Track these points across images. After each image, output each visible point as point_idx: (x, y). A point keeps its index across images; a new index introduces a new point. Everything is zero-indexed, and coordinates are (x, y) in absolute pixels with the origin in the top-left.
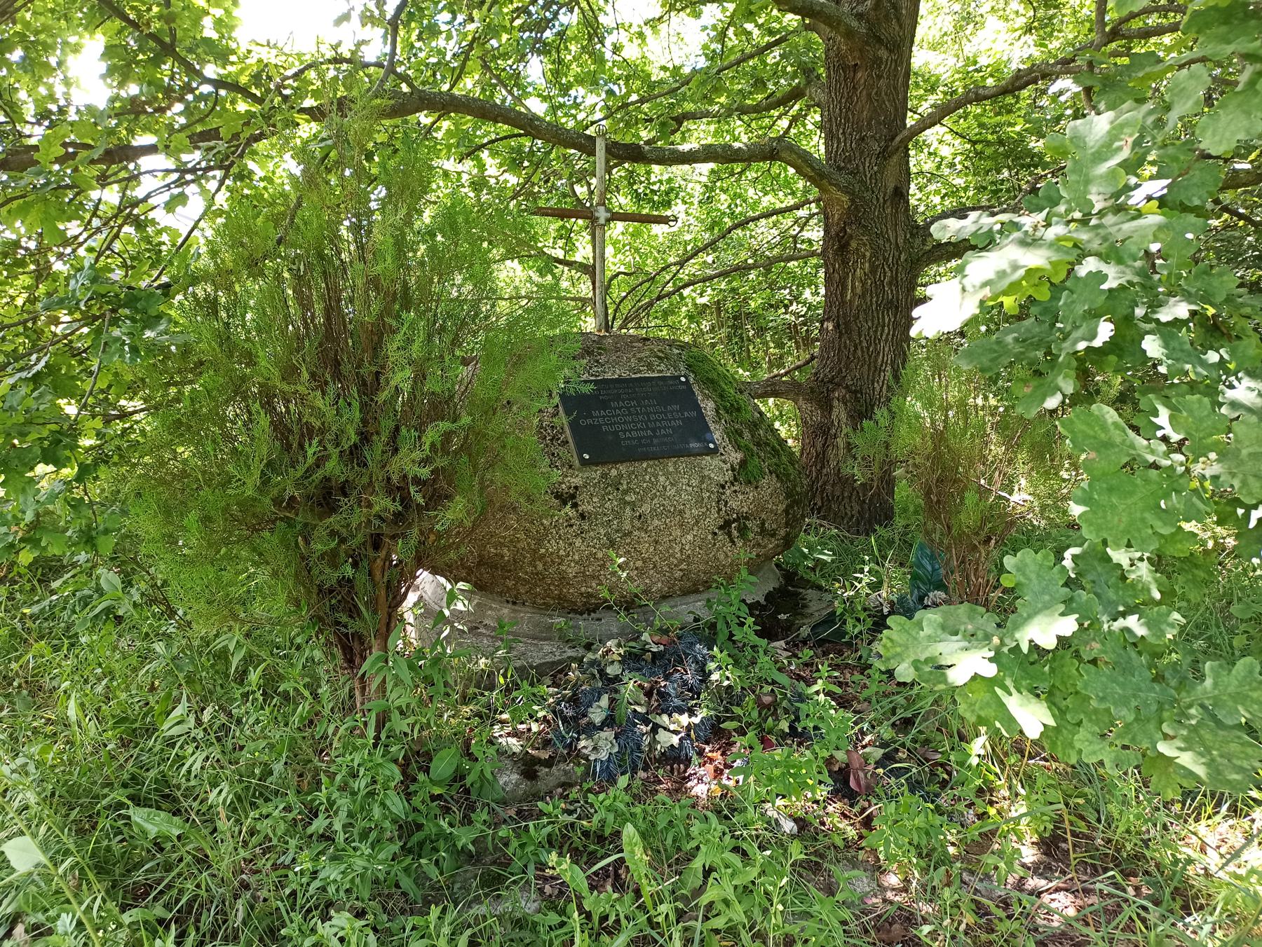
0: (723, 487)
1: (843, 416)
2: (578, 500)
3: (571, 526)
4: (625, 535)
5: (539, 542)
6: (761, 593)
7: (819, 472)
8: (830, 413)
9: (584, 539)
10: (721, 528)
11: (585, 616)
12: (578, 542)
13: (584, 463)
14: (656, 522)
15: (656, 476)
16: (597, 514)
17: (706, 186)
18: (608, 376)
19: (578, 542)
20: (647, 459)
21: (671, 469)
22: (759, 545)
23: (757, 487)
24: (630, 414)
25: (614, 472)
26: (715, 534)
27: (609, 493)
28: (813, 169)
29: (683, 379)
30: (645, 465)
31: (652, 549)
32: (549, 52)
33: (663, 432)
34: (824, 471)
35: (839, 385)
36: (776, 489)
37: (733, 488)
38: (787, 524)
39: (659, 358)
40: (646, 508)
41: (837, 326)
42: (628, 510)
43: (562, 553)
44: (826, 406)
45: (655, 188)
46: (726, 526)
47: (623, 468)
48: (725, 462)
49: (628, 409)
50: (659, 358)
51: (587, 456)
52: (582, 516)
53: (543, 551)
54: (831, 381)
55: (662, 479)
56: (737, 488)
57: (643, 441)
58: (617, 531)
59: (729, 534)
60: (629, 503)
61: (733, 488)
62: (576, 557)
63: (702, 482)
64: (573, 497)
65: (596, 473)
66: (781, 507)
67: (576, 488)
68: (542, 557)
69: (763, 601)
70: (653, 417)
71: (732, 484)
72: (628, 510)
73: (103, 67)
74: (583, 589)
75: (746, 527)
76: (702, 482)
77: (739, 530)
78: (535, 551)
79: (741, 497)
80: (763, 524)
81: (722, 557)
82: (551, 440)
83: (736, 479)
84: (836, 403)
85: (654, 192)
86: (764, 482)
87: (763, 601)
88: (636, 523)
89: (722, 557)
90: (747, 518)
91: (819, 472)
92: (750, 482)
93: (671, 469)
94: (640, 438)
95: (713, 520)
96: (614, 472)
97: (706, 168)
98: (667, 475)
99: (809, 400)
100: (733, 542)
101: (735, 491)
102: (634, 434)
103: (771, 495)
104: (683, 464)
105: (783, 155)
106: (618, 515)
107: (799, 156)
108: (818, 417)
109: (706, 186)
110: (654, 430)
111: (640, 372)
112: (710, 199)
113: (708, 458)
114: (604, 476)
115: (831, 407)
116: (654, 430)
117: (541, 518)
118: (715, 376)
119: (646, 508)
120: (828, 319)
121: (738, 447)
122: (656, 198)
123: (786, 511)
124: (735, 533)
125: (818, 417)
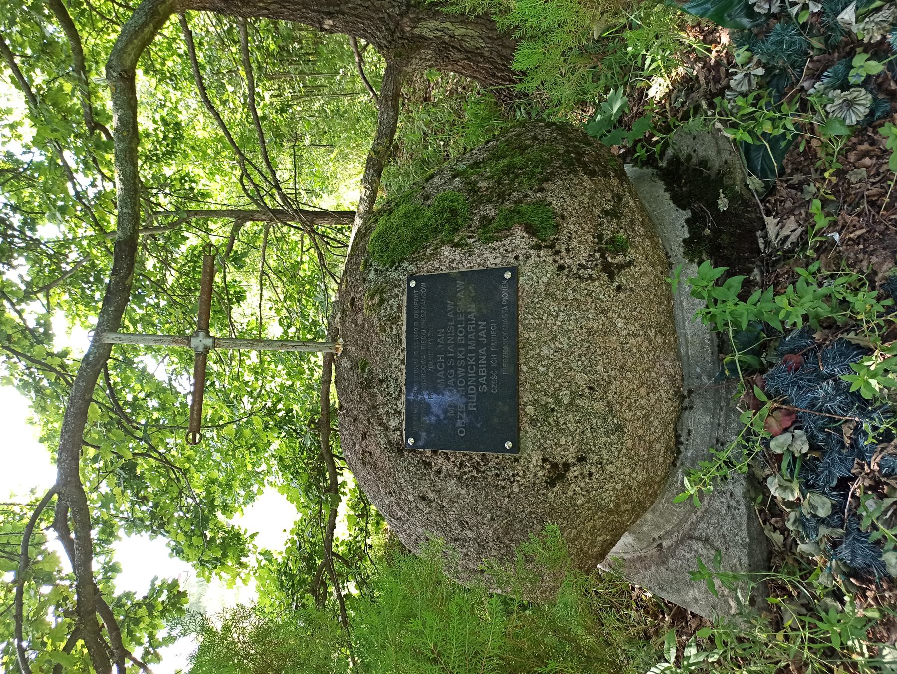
0: (561, 268)
1: (432, 24)
2: (560, 461)
3: (591, 474)
4: (611, 411)
5: (600, 508)
6: (674, 214)
7: (487, 60)
8: (426, 39)
9: (610, 462)
10: (611, 277)
11: (682, 448)
12: (611, 468)
13: (516, 448)
14: (599, 368)
15: (541, 358)
16: (580, 442)
17: (160, 80)
18: (402, 378)
19: (611, 468)
20: (517, 365)
21: (533, 335)
22: (632, 222)
23: (563, 217)
24: (455, 368)
25: (530, 410)
26: (619, 288)
27: (557, 422)
28: (145, 25)
29: (413, 284)
30: (524, 368)
31: (630, 376)
32: (33, 220)
33: (483, 333)
34: (487, 54)
35: (397, 24)
36: (564, 188)
37: (564, 253)
38: (606, 176)
39: (381, 302)
40: (581, 380)
41: (330, 15)
42: (579, 402)
43: (619, 486)
44: (419, 42)
45: (161, 135)
46: (610, 270)
47: (525, 397)
48: (528, 257)
49: (447, 368)
50: (381, 302)
51: (508, 445)
52: (581, 459)
53: (612, 506)
54: (392, 33)
55: (545, 351)
56: (563, 247)
57: (494, 365)
58: (605, 420)
59: (621, 267)
60: (572, 400)
61: (564, 253)
62: (628, 471)
63: (553, 296)
64: (555, 466)
65: (529, 433)
66: (588, 183)
67: (544, 460)
68: (618, 505)
69: (688, 214)
70: (461, 340)
71: (557, 253)
72: (579, 402)
73: (58, 555)
74: (661, 460)
75: (612, 241)
76: (553, 296)
77: (615, 253)
78: (610, 512)
79: (574, 243)
80: (606, 213)
81: (646, 280)
82: (478, 471)
83: (552, 246)
84: (417, 31)
85: (166, 137)
86: (555, 204)
87: (688, 214)
88: (598, 394)
89: (646, 280)
90: (600, 237)
91: (487, 60)
92: (556, 226)
93: (533, 335)
94: (489, 367)
95: (601, 288)
96: (530, 410)
97: (143, 81)
98: (541, 343)
99: (408, 59)
100: (630, 263)
101: (567, 250)
102: (483, 372)
103: (572, 196)
104: (526, 318)
105: (128, 63)
106: (586, 417)
107: (129, 42)
108: (428, 53)
109: (160, 80)
110: (480, 345)
111: (398, 335)
112: (173, 77)
113: (521, 280)
114: (533, 422)
115: (421, 37)
116: (480, 345)
117: (575, 505)
118: (405, 232)
119: (581, 380)
120: (321, 23)
121: (506, 230)
122: (171, 135)
123: (592, 174)
124: (619, 259)
125: (428, 53)
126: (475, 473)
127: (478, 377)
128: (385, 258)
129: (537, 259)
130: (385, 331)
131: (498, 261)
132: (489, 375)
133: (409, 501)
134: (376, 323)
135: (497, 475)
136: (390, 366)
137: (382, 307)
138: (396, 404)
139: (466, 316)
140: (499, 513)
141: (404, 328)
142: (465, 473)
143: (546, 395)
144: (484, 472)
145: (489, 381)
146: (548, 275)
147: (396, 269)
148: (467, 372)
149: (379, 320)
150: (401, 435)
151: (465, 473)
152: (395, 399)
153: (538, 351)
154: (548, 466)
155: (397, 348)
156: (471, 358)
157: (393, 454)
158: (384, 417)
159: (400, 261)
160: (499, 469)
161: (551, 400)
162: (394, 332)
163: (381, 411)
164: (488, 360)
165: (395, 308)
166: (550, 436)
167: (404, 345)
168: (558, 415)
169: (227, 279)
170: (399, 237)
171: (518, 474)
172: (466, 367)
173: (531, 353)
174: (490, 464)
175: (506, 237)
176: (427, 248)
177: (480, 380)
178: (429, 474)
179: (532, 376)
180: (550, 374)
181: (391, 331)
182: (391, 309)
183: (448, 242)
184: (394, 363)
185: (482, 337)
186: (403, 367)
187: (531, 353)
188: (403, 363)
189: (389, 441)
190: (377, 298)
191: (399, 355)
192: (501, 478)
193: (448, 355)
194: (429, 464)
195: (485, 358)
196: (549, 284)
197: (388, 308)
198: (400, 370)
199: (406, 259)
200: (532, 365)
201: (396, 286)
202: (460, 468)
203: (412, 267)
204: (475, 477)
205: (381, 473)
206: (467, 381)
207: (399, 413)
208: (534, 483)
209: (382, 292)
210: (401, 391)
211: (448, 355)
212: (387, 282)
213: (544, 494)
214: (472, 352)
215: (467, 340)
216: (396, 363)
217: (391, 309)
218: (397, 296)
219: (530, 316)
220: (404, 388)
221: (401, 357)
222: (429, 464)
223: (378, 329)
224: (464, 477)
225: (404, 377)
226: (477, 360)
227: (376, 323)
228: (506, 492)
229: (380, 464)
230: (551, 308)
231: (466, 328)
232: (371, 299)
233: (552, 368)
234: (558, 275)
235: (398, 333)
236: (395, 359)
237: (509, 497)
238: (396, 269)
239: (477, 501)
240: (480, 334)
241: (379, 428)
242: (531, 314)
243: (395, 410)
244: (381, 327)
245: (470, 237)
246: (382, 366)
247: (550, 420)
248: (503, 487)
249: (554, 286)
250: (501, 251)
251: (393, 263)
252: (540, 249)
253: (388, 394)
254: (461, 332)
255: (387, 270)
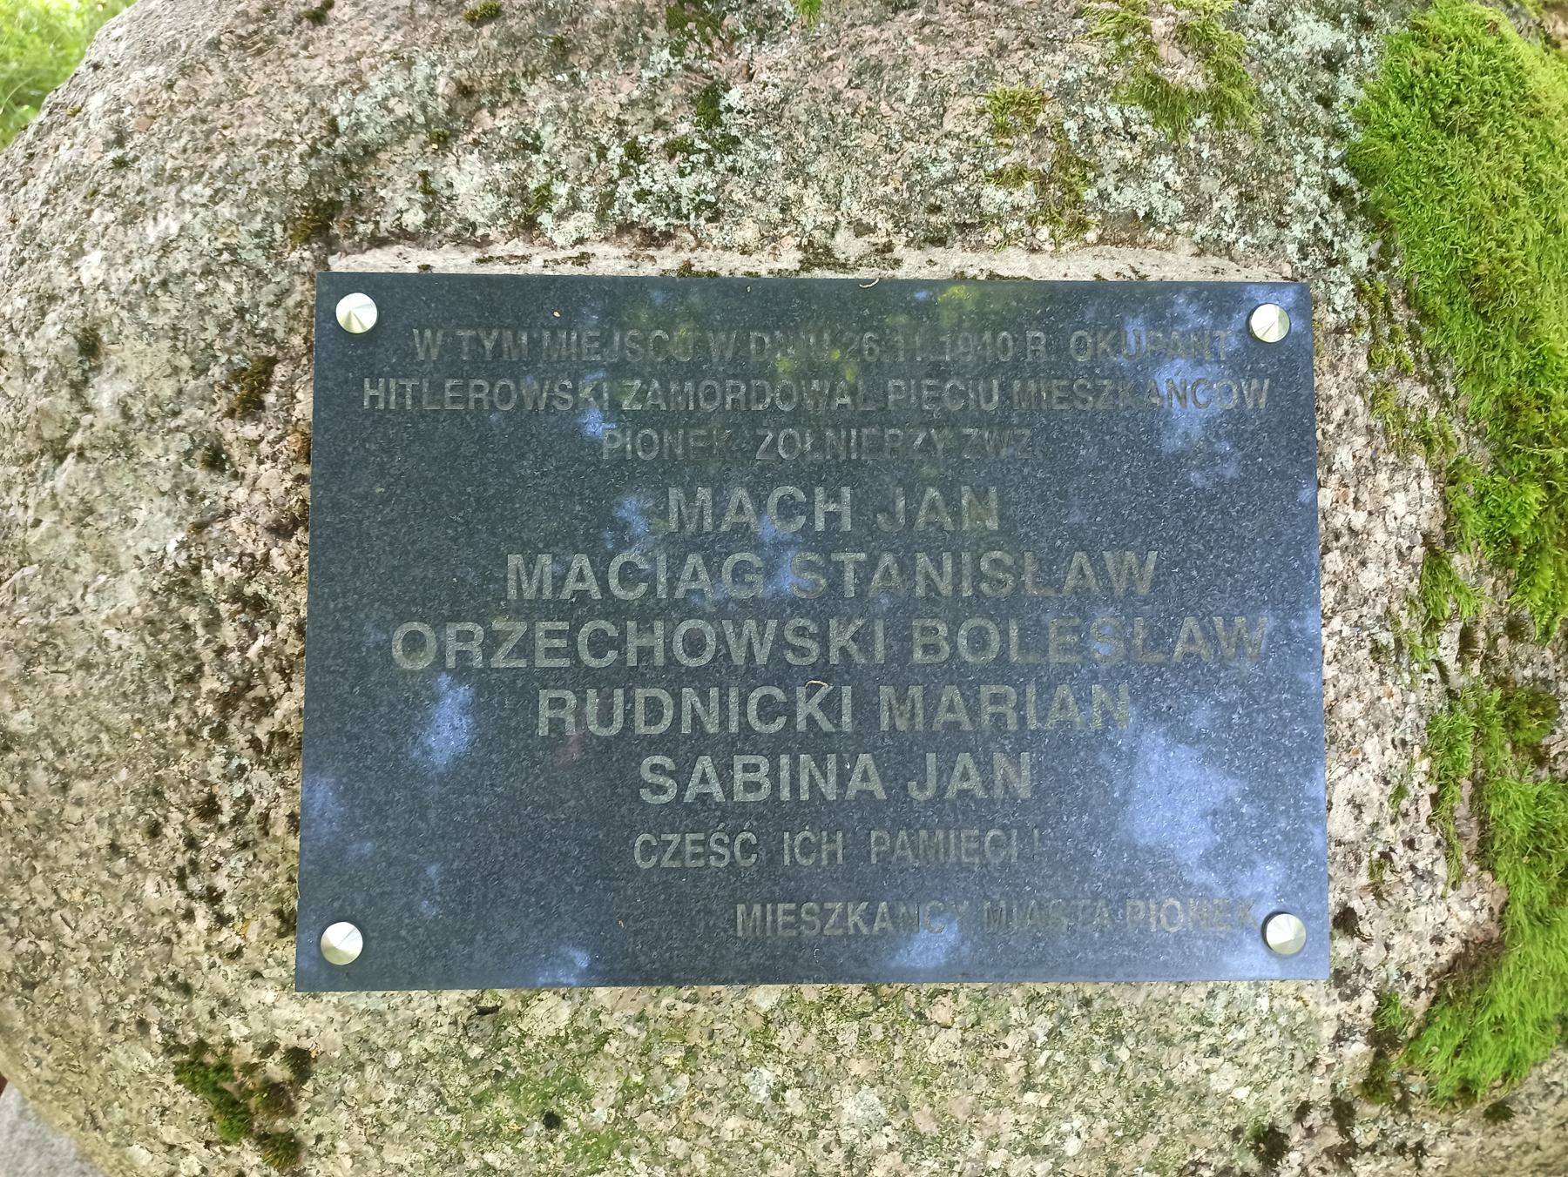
27: (494, 1133)
64: (278, 1098)
67: (300, 1060)
126: (209, 684)
127: (726, 748)
128: (1405, 116)
129: (1328, 1031)
130: (1000, 130)
131: (1340, 822)
132: (731, 815)
133: (78, 252)
134: (1050, 70)
135: (209, 809)
136: (798, 171)
137: (1137, 112)
138: (575, 205)
139: (1066, 672)
140: (39, 776)
141: (1014, 264)
142: (213, 623)
143: (628, 1093)
144: (220, 734)
145: (697, 814)
146: (1241, 1093)
147: (1336, 192)
148: (751, 675)
149: (1066, 92)
150: (402, 235)
151: (213, 623)
152: (608, 200)
153: (858, 1068)
154: (276, 1069)
155: (900, 217)
156: (830, 706)
157: (298, 178)
158: (504, 122)
159: (1378, 223)
160: (237, 821)
161: (601, 1113)
162: (994, 196)
163: (541, 96)
164: (814, 811)
165: (1128, 197)
166: (421, 1099)
167: (913, 264)
168: (528, 1144)
169: (51, 1079)
170: (1502, 203)
171: (222, 920)
172: (781, 674)
173: (849, 1035)
174: (259, 775)
175: (1446, 846)
176: (1433, 381)
177: (705, 764)
178: (207, 400)
179: (728, 1030)
180: (733, 1123)
181: (999, 177)
182: (1127, 172)
183: (1452, 517)
184: (812, 200)
185: (946, 769)
186: (789, 259)
187: (849, 1035)
188: (817, 254)
189: (369, 152)
190: (1187, 73)
191: (861, 229)
192: (197, 826)
193: (850, 558)
194: (250, 407)
195: (830, 790)
196: (1198, 1098)
197: (1127, 153)
198: (770, 237)
199: (1381, 262)
200: (785, 1038)
201: (1247, 197)
202: (236, 596)
203: (1342, 295)
204: (191, 679)
205: (212, 82)
206: (699, 678)
207: (529, 226)
208: (186, 989)
209: (1219, 105)
210: (653, 239)
211: (850, 558)
212: (1269, 131)
213: (143, 1025)
214: (865, 708)
215: (932, 679)
216: (813, 211)
217: (1127, 172)
218: (1195, 212)
219: (1042, 1025)
220: (667, 261)
221: (847, 245)
222: (250, 407)
223: (1009, 83)
224: (193, 615)
225: (732, 264)
226: (818, 743)
227: (1050, 70)
228: (134, 839)
229: (260, 80)
230: (1078, 1121)
231: (1001, 669)
232: (1183, 34)
233: (769, 1133)
234: (1236, 1133)
235: (984, 221)
236: (834, 202)
237: (114, 848)
238: (1336, 192)
239: (86, 665)
240: (965, 760)
241: (442, 86)
242: (1054, 1035)
243: (544, 198)
244: (1025, 105)
245: (1466, 639)
246: (798, 109)
247: (502, 1105)
248: (154, 831)
249: (1185, 1120)
250: (1389, 832)
251: (1367, 174)
252: (1375, 1038)
253: (635, 152)
254: (979, 641)
255: (1337, 134)
